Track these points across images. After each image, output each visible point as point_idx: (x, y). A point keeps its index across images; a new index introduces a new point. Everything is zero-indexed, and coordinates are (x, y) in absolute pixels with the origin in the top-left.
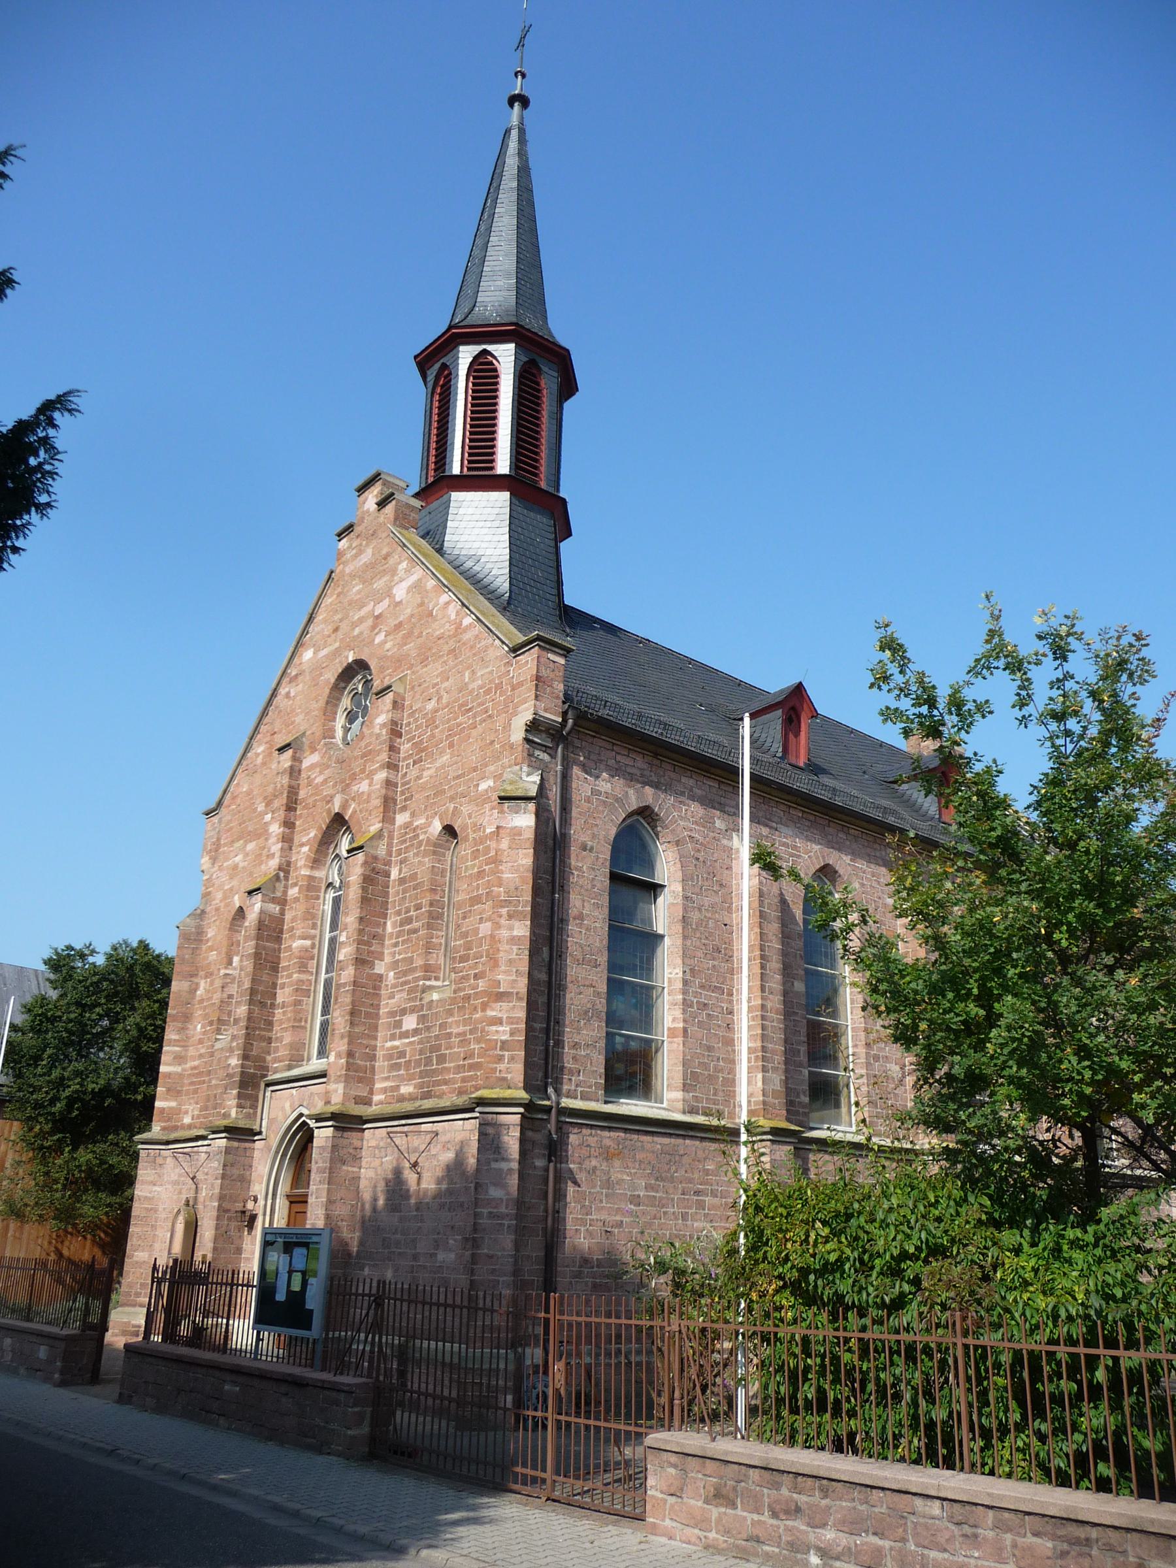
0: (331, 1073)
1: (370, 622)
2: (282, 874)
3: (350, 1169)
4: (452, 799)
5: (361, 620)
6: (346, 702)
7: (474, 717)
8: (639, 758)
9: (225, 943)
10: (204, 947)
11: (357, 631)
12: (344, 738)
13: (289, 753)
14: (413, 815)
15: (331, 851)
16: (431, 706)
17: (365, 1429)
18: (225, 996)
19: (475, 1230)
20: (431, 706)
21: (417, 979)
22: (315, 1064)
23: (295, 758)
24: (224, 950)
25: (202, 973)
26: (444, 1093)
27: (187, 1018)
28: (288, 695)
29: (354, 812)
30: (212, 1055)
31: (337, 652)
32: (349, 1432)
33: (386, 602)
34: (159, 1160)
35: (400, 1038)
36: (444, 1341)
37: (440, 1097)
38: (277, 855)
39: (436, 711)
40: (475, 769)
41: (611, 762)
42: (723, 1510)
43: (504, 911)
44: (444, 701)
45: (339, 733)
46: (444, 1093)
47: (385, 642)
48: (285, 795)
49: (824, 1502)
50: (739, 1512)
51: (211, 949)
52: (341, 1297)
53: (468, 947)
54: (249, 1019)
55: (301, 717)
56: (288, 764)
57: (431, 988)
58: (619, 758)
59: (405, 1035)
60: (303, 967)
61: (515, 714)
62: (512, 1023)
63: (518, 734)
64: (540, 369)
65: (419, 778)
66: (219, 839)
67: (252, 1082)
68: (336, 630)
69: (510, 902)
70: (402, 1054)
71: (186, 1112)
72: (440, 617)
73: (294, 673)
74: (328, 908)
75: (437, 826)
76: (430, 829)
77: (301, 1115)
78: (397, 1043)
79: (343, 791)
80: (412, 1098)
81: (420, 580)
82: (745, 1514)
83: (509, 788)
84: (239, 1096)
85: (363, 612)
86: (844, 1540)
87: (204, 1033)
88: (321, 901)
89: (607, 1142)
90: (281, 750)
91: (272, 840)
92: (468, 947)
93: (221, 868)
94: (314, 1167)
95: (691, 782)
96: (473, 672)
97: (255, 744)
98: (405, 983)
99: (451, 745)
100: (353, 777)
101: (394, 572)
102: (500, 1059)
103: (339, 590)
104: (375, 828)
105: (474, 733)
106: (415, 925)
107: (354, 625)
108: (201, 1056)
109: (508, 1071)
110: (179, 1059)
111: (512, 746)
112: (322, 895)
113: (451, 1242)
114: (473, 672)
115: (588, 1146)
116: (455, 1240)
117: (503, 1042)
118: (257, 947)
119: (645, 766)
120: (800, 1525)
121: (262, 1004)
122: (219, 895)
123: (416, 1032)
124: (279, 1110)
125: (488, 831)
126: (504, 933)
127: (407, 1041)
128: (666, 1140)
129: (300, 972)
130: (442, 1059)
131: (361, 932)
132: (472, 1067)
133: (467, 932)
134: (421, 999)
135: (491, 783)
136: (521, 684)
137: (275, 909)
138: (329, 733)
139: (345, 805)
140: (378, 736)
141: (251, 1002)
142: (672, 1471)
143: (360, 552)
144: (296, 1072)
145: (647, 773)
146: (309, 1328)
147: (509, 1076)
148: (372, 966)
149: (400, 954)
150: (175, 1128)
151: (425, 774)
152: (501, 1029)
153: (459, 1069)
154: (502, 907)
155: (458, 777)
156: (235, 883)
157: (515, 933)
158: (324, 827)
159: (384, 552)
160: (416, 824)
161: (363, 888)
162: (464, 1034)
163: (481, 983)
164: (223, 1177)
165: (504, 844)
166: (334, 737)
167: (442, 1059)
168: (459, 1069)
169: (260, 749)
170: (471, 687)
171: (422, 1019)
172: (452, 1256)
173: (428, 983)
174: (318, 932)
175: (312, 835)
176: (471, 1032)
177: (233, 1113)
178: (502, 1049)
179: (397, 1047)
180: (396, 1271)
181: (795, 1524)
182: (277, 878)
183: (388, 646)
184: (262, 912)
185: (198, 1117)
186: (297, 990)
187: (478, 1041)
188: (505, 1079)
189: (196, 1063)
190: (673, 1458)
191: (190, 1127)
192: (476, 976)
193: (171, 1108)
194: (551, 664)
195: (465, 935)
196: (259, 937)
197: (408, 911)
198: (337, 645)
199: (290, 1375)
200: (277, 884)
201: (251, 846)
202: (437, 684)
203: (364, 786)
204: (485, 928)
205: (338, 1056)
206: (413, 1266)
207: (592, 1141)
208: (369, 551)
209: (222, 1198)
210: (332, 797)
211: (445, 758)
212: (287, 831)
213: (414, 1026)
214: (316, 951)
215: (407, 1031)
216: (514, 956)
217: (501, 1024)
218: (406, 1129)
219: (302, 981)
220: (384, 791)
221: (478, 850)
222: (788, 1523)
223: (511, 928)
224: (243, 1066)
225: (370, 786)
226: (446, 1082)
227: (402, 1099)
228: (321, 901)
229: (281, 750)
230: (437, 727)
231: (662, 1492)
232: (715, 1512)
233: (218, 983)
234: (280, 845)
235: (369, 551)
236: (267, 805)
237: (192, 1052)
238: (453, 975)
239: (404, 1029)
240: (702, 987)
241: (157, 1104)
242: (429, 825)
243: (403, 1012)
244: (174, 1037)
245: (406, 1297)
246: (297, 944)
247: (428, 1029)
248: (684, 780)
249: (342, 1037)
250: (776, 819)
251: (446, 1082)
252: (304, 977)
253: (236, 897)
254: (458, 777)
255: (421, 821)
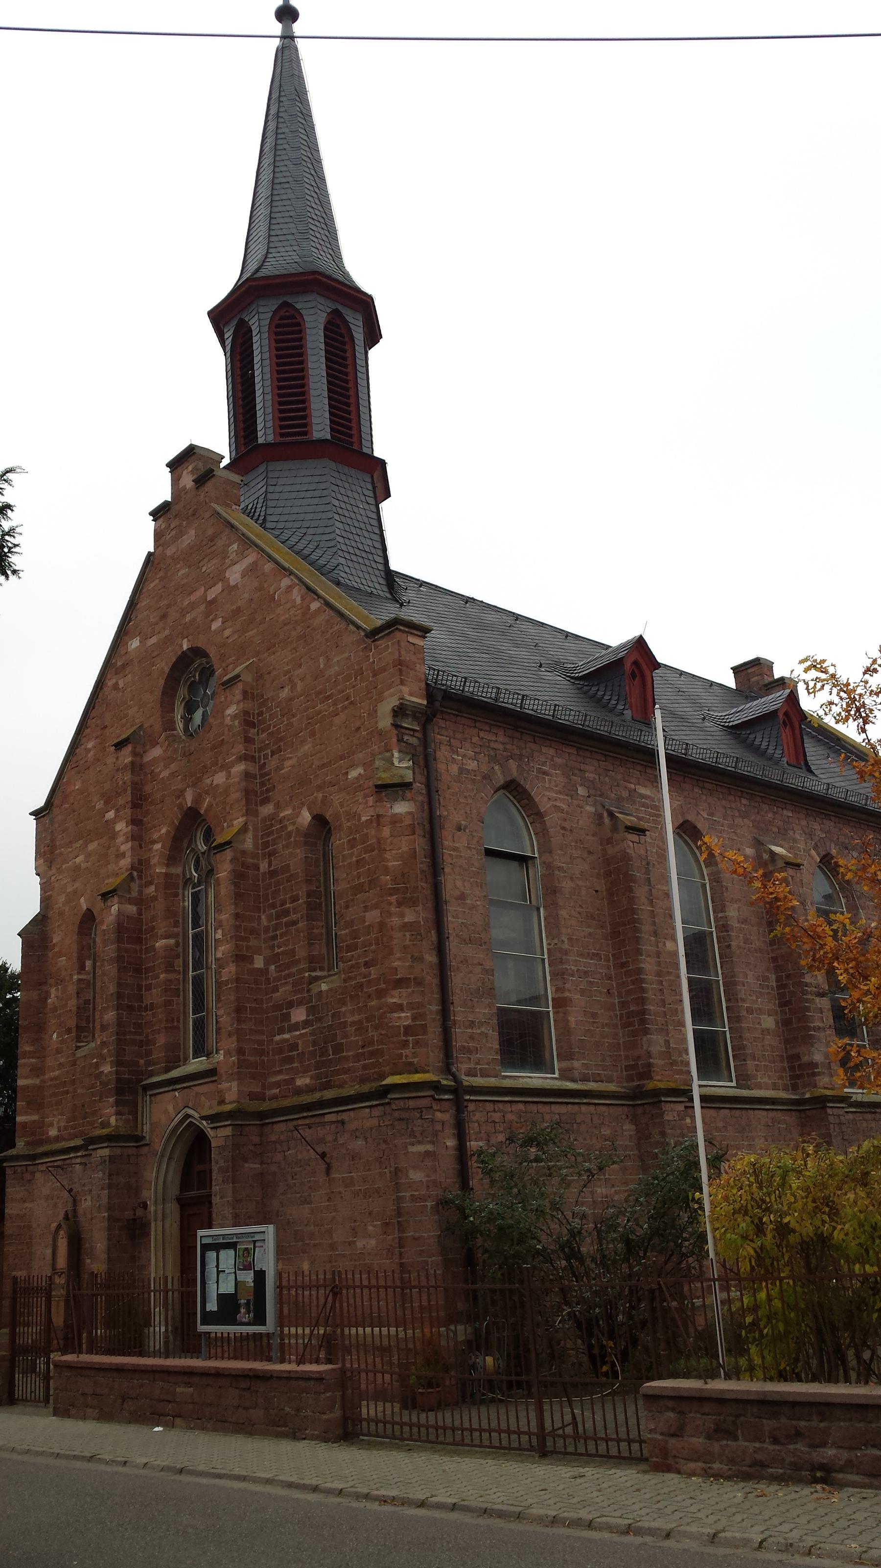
0: (222, 1070)
1: (202, 607)
2: (135, 874)
3: (252, 1166)
4: (320, 788)
5: (193, 606)
6: (183, 692)
7: (335, 704)
8: (501, 733)
9: (74, 947)
10: (50, 954)
11: (188, 618)
12: (186, 729)
13: (129, 749)
14: (278, 806)
15: (185, 845)
16: (284, 694)
17: (337, 1414)
18: (81, 1001)
19: (399, 1214)
20: (284, 694)
21: (301, 971)
22: (196, 1064)
23: (134, 754)
24: (75, 955)
25: (51, 981)
26: (345, 1083)
27: (40, 1028)
28: (116, 687)
29: (210, 806)
30: (74, 1063)
31: (167, 641)
32: (324, 1417)
33: (219, 587)
34: (27, 1176)
35: (290, 1031)
36: (372, 1326)
37: (341, 1086)
38: (128, 854)
39: (291, 699)
40: (342, 758)
41: (475, 740)
42: (725, 1442)
43: (393, 899)
44: (299, 688)
45: (180, 725)
46: (345, 1083)
47: (222, 629)
48: (129, 792)
49: (822, 1425)
50: (742, 1443)
51: (60, 954)
52: (293, 1292)
53: (355, 935)
54: (119, 1024)
55: (135, 709)
56: (128, 760)
57: (318, 979)
58: (482, 734)
59: (296, 1027)
60: (170, 967)
61: (381, 699)
62: (413, 1009)
63: (385, 722)
64: (297, 310)
65: (279, 768)
66: (53, 841)
67: (131, 1089)
68: (164, 617)
69: (398, 889)
70: (294, 1046)
71: (51, 1125)
72: (283, 602)
73: (119, 664)
74: (188, 903)
75: (306, 817)
76: (300, 820)
77: (188, 1116)
78: (287, 1036)
79: (194, 785)
80: (310, 1089)
81: (255, 564)
82: (746, 1444)
83: (384, 775)
84: (117, 1103)
85: (193, 598)
86: (845, 1455)
87: (62, 1042)
88: (180, 897)
89: (510, 1117)
90: (119, 746)
91: (120, 839)
92: (355, 935)
93: (60, 871)
94: (215, 1168)
95: (551, 752)
96: (328, 659)
97: (83, 740)
98: (289, 976)
99: (313, 734)
100: (205, 770)
101: (224, 555)
102: (405, 1044)
103: (161, 574)
104: (238, 822)
105: (337, 720)
106: (294, 917)
107: (183, 612)
108: (61, 1065)
109: (415, 1055)
110: (37, 1071)
111: (380, 733)
112: (180, 891)
113: (370, 1228)
114: (328, 659)
115: (494, 1122)
116: (374, 1226)
117: (406, 1028)
118: (119, 949)
119: (507, 740)
120: (801, 1447)
121: (130, 1008)
122: (62, 898)
123: (306, 1024)
124: (164, 1113)
125: (364, 819)
126: (396, 921)
127: (298, 1033)
128: (563, 1109)
129: (166, 972)
130: (338, 1049)
131: (237, 928)
132: (372, 1054)
133: (352, 921)
134: (308, 991)
135: (360, 770)
136: (383, 669)
137: (132, 909)
138: (169, 725)
139: (198, 799)
140: (230, 728)
141: (119, 1007)
142: (671, 1414)
143: (181, 533)
144: (175, 1073)
145: (508, 746)
146: (264, 1324)
147: (415, 1060)
148: (252, 962)
149: (279, 947)
150: (41, 1142)
151: (288, 763)
152: (403, 1015)
153: (358, 1057)
154: (391, 895)
155: (324, 766)
156: (78, 884)
157: (406, 920)
158: (177, 822)
159: (210, 532)
160: (282, 815)
161: (236, 885)
162: (360, 1022)
163: (373, 970)
164: (110, 1186)
165: (386, 832)
166: (175, 729)
167: (338, 1049)
168: (358, 1057)
169: (90, 745)
170: (327, 673)
171: (311, 1011)
172: (373, 1242)
173: (314, 974)
174: (180, 929)
175: (164, 831)
176: (368, 1019)
177: (113, 1120)
178: (406, 1034)
179: (287, 1040)
180: (312, 1263)
181: (797, 1446)
182: (131, 878)
183: (227, 633)
184: (120, 913)
185: (66, 1128)
186: (166, 990)
187: (376, 1028)
188: (411, 1064)
189: (57, 1073)
190: (670, 1404)
191: (57, 1139)
192: (367, 965)
193: (34, 1121)
194: (412, 648)
195: (351, 923)
196: (119, 940)
197: (283, 903)
198: (167, 632)
199: (250, 1369)
200: (132, 885)
201: (92, 846)
202: (288, 672)
203: (219, 779)
204: (372, 916)
205: (228, 1053)
206: (331, 1256)
207: (497, 1117)
208: (192, 532)
209: (110, 1208)
210: (183, 791)
211: (307, 747)
212: (135, 828)
213: (304, 1017)
214: (180, 949)
215: (297, 1023)
216: (407, 942)
217: (402, 1010)
218: (307, 1121)
219: (170, 981)
220: (244, 784)
221: (355, 839)
222: (791, 1447)
223: (402, 915)
224: (117, 1073)
225: (228, 777)
226: (346, 1071)
227: (299, 1091)
228: (180, 897)
229: (119, 746)
230: (293, 716)
231: (662, 1434)
232: (716, 1447)
233: (72, 989)
234: (129, 844)
235: (192, 532)
236: (106, 803)
237: (50, 1062)
238: (341, 965)
239: (293, 1021)
240: (581, 955)
241: (19, 1119)
242: (298, 815)
243: (291, 1005)
244: (27, 1049)
245: (382, 1283)
246: (160, 944)
247: (319, 1019)
248: (544, 750)
249: (230, 1035)
250: (633, 780)
251: (346, 1071)
252: (171, 976)
253: (82, 900)
254: (324, 766)
255: (288, 812)
